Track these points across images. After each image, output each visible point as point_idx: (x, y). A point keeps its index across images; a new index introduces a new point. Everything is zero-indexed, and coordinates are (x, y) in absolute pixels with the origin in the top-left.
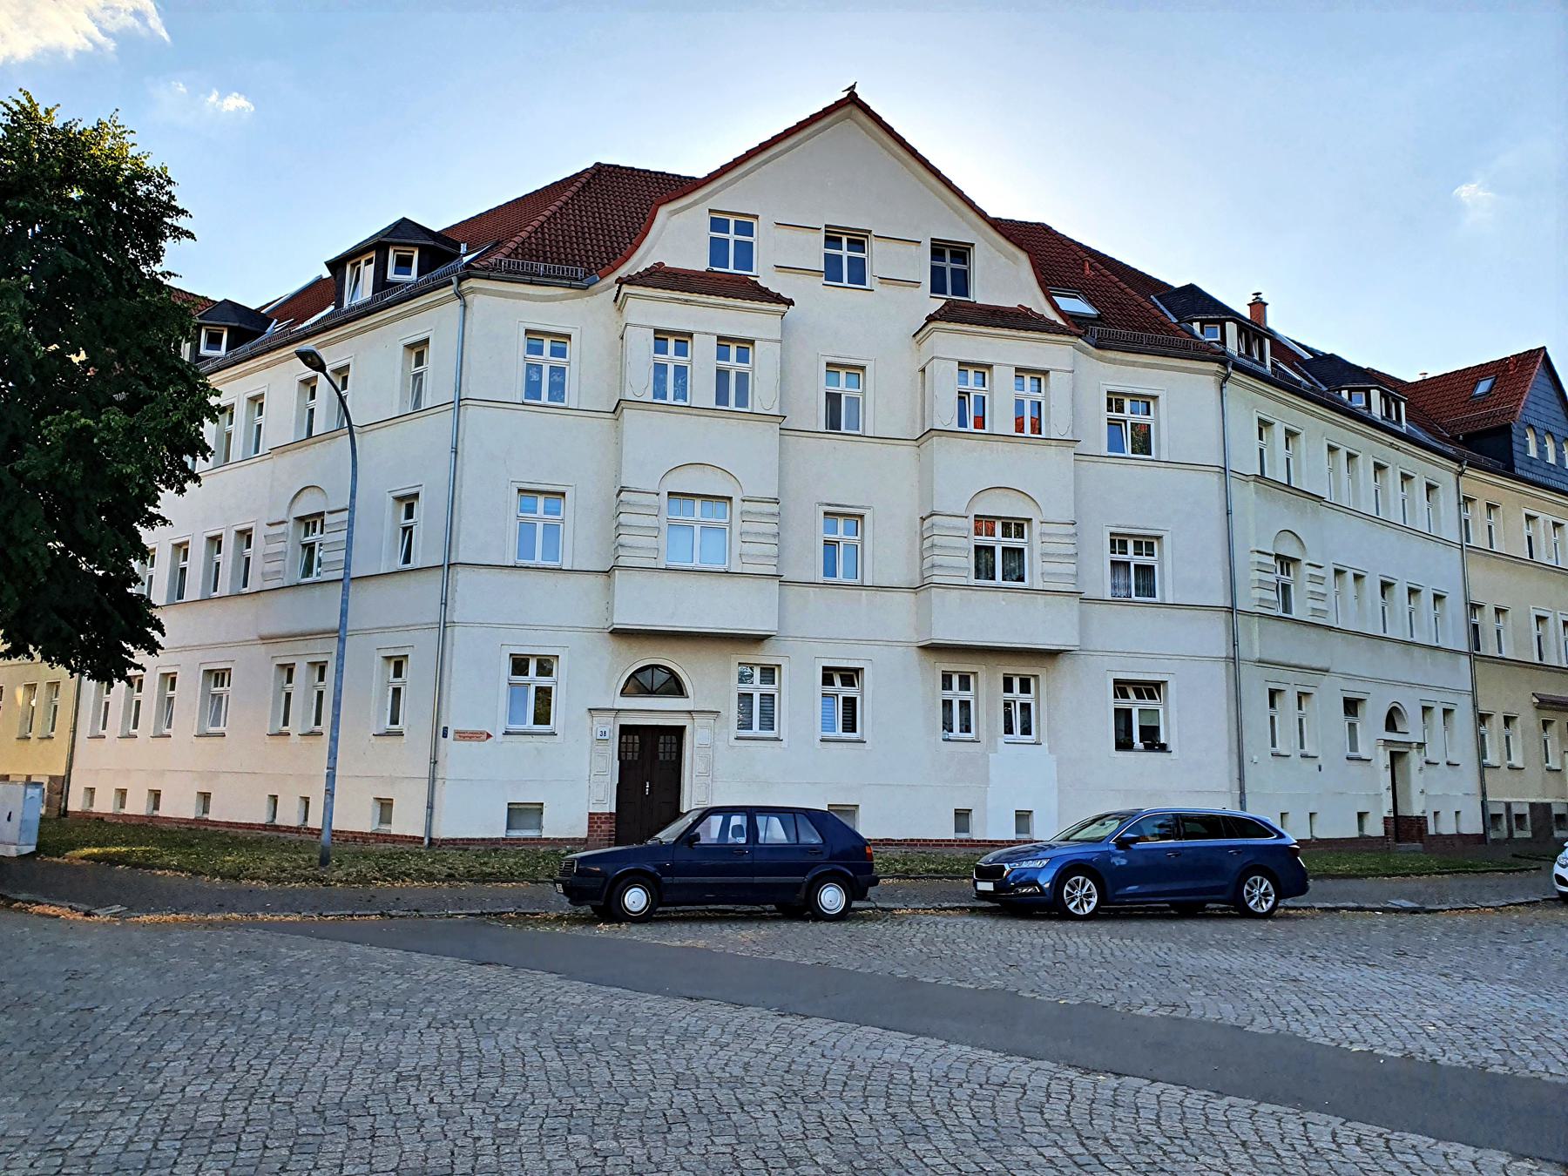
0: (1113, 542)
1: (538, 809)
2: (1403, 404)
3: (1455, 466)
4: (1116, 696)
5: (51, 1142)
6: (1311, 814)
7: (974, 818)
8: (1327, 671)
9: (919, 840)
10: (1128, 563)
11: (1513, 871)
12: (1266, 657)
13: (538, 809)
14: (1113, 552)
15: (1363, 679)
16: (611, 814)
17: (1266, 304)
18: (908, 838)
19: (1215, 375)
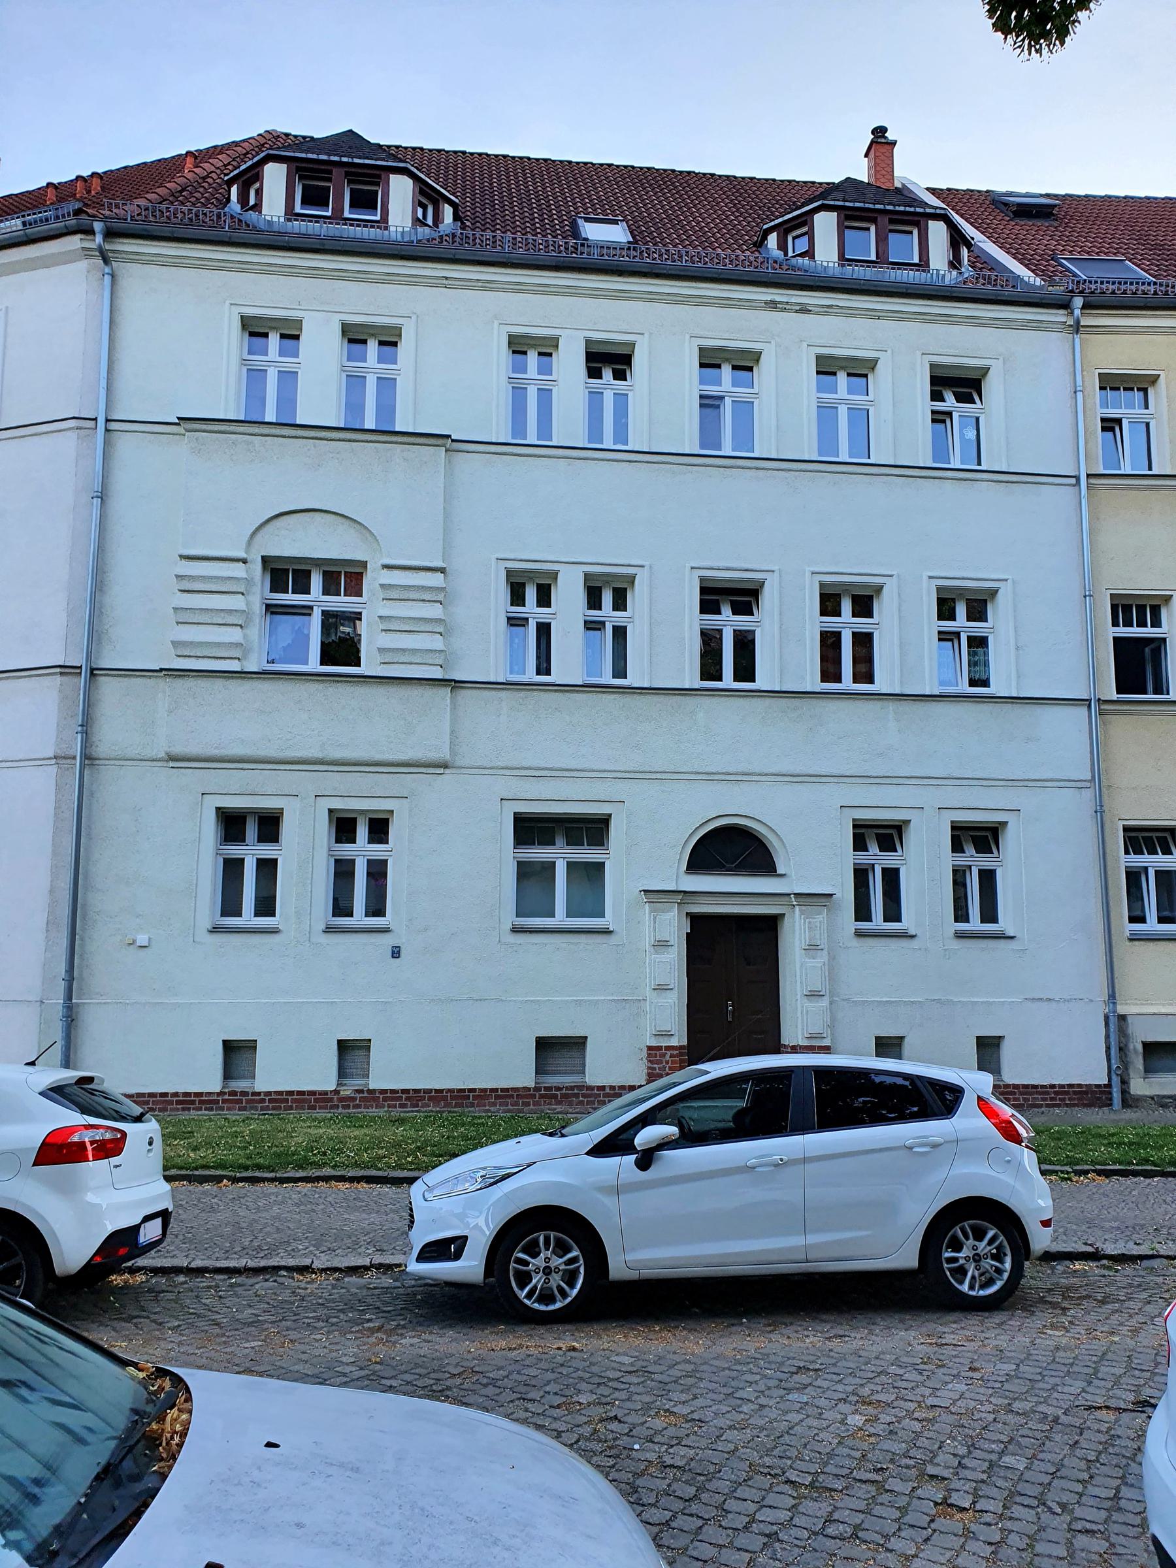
0: (1114, 608)
1: (579, 1043)
2: (765, 227)
3: (1059, 316)
4: (1127, 852)
5: (835, 1365)
6: (344, 1046)
7: (1007, 1052)
8: (446, 766)
9: (269, 1093)
10: (958, 634)
11: (326, 1179)
12: (179, 749)
13: (579, 1043)
14: (1115, 624)
15: (601, 775)
16: (681, 1047)
17: (894, 143)
18: (171, 1090)
19: (87, 256)
